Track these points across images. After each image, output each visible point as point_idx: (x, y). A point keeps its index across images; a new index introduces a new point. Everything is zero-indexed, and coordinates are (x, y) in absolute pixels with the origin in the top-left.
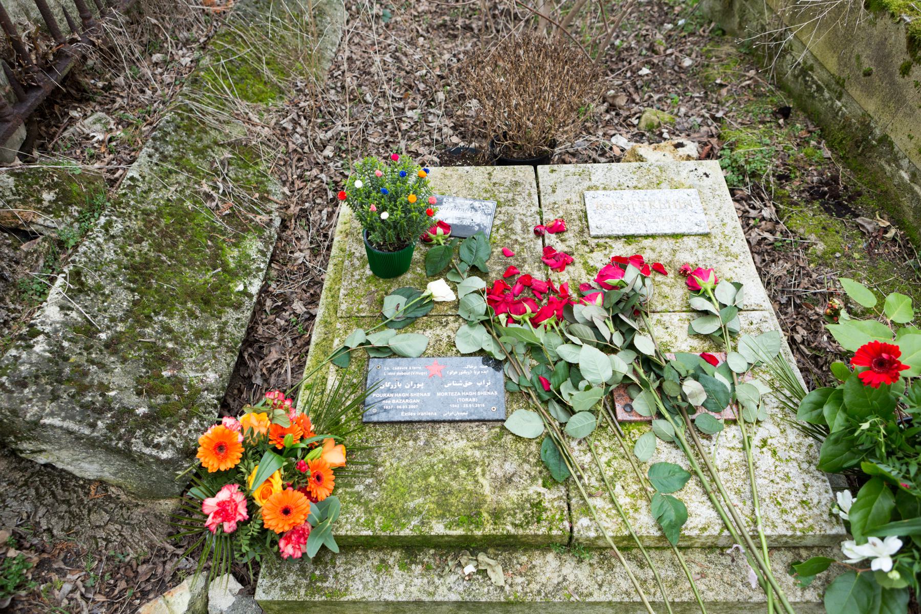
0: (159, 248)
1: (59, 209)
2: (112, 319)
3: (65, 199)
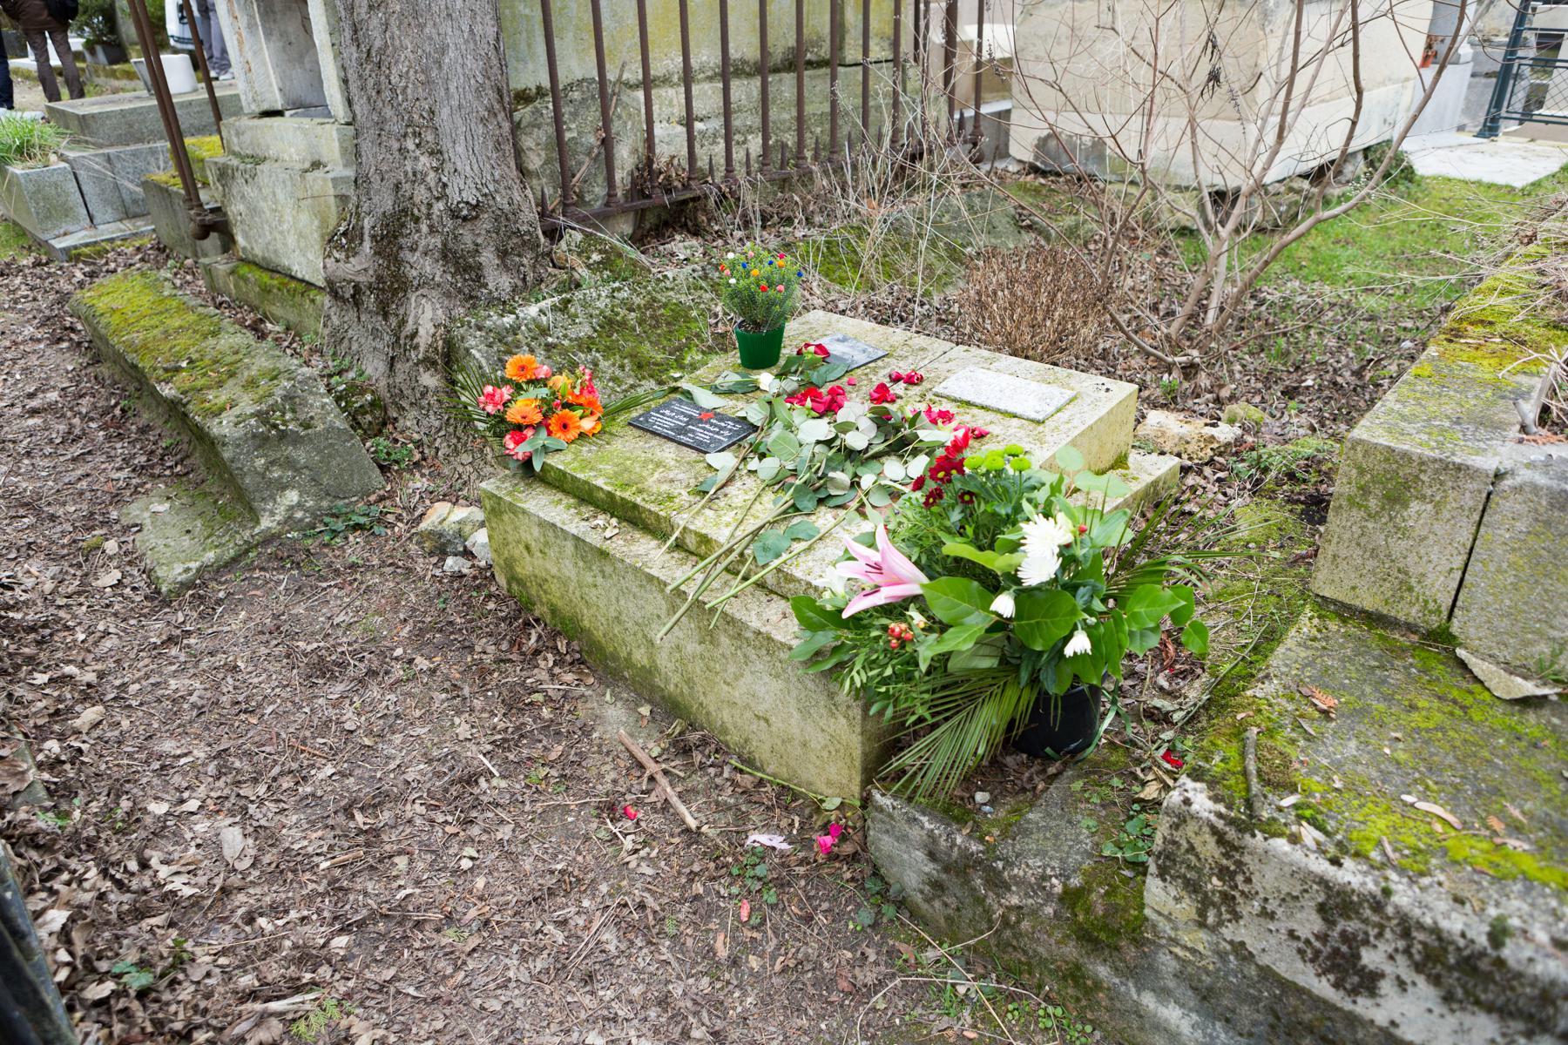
0: (641, 322)
1: (598, 269)
2: (565, 336)
3: (605, 264)
